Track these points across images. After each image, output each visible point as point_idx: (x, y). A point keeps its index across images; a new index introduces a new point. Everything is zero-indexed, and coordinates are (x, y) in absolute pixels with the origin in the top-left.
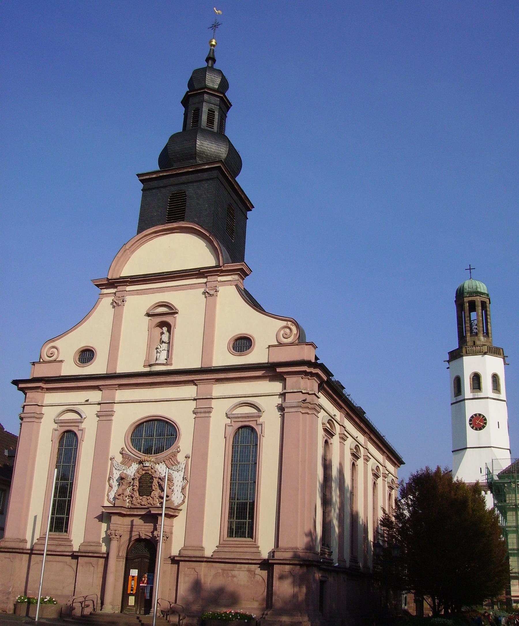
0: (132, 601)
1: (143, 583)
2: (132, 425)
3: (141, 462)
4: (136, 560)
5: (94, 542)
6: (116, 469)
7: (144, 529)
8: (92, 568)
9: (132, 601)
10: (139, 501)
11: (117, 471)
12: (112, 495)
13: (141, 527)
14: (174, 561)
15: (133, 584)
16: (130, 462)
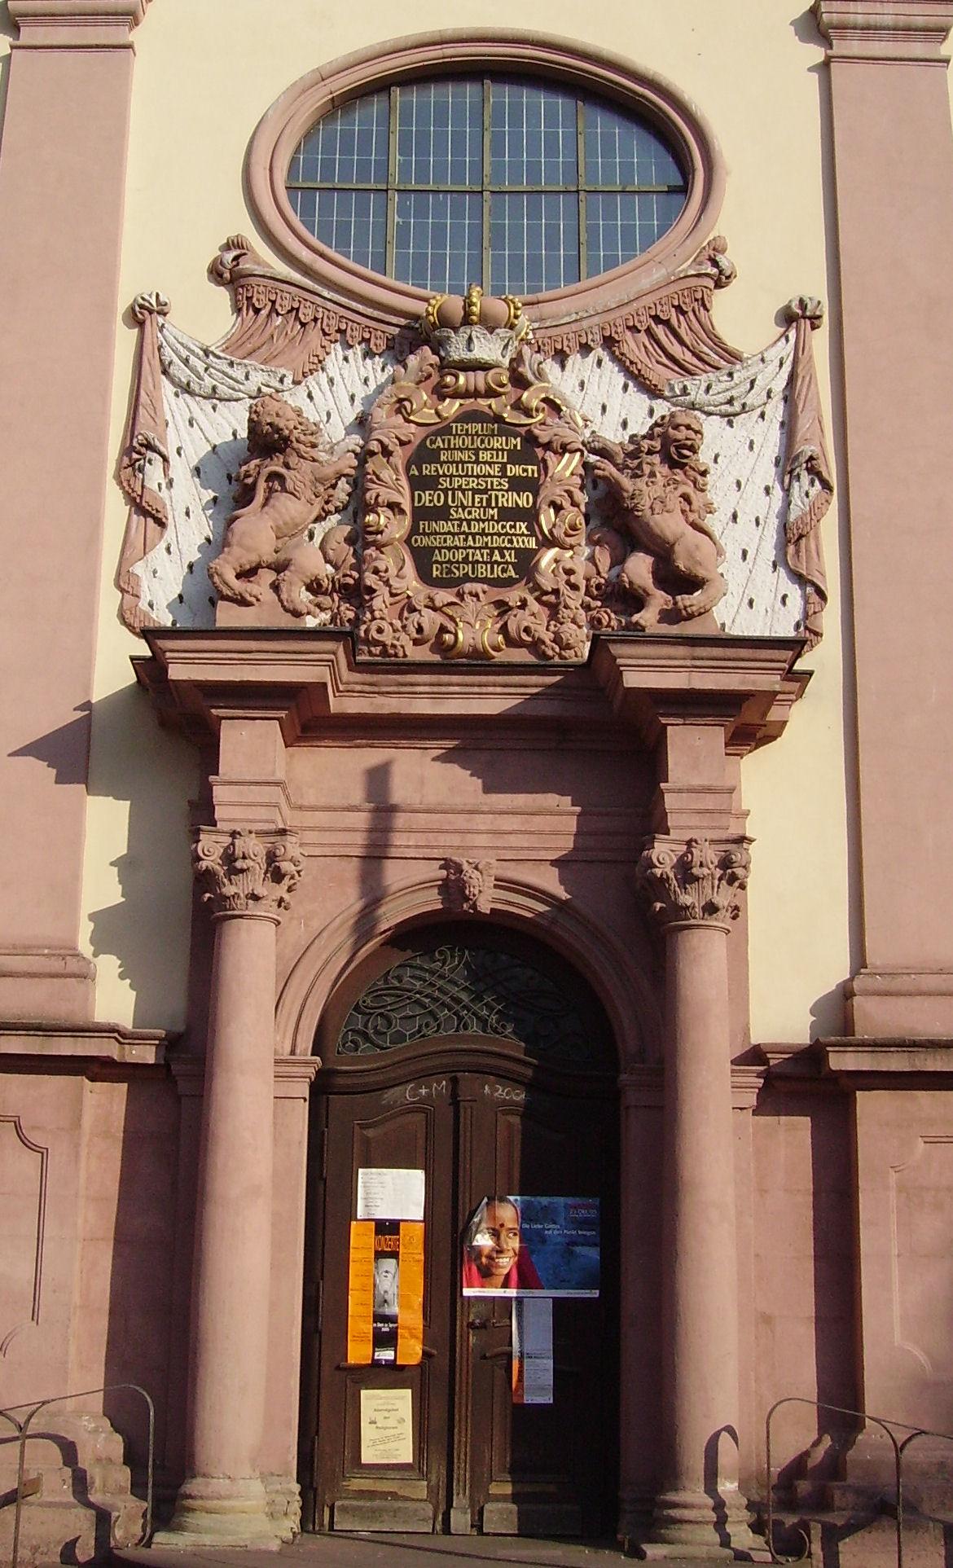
0: (387, 1425)
1: (486, 1274)
2: (302, 88)
3: (414, 336)
4: (406, 1094)
5: (26, 950)
6: (187, 389)
7: (513, 843)
8: (29, 1162)
9: (387, 1425)
10: (430, 620)
11: (199, 408)
12: (163, 587)
13: (460, 821)
14: (807, 1084)
15: (390, 1286)
16: (314, 334)
